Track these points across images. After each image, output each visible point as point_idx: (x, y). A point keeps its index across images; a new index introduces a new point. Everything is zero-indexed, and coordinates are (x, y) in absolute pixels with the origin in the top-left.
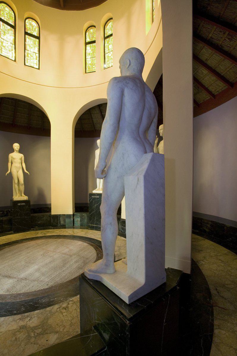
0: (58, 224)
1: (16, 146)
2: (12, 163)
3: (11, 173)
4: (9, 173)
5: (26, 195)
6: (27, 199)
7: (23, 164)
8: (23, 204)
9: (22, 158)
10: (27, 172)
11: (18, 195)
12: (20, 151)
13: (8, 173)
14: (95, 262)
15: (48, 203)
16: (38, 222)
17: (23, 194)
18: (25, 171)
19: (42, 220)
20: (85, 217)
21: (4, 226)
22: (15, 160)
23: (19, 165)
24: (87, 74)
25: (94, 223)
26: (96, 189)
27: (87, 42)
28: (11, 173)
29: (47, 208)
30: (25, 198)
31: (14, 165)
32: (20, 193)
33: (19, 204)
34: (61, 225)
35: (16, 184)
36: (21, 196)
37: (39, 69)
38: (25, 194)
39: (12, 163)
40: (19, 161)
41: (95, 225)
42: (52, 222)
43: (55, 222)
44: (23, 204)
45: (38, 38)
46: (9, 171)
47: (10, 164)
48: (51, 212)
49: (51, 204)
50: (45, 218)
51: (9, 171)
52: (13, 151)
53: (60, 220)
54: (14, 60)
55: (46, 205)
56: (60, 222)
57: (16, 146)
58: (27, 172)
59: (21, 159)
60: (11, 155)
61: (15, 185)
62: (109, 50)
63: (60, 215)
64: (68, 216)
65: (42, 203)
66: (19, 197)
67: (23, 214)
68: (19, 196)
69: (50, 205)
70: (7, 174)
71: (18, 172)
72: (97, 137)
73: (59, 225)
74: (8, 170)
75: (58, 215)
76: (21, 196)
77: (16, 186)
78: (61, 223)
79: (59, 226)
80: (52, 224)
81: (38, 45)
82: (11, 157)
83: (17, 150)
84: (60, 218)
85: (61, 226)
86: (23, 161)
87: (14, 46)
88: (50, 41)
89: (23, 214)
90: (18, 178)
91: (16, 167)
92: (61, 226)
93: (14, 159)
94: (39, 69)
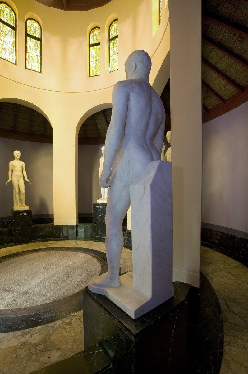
0: (61, 235)
1: (17, 153)
2: (12, 172)
3: (11, 182)
4: (10, 182)
5: (27, 205)
6: (29, 209)
7: (24, 172)
8: (24, 214)
9: (23, 166)
10: (28, 181)
11: (19, 204)
12: (21, 159)
13: (8, 181)
14: (99, 275)
15: (50, 213)
16: (40, 233)
17: (24, 204)
18: (27, 179)
19: (44, 232)
20: (89, 228)
21: (4, 237)
22: (16, 168)
23: (20, 173)
24: (91, 77)
25: (99, 234)
26: (101, 199)
27: (91, 44)
28: (11, 182)
29: (49, 219)
30: (26, 208)
31: (14, 173)
32: (21, 203)
33: (20, 215)
34: (64, 236)
35: (17, 193)
36: (22, 206)
37: (41, 72)
38: (26, 204)
39: (12, 172)
40: (20, 169)
41: (99, 237)
42: (54, 233)
43: (58, 233)
44: (24, 214)
45: (40, 40)
46: (9, 180)
47: (10, 172)
48: (53, 223)
49: (53, 214)
50: (47, 229)
51: (9, 180)
52: (13, 158)
53: (63, 231)
54: (14, 63)
55: (48, 215)
56: (63, 233)
57: (17, 153)
58: (28, 181)
59: (22, 167)
60: (12, 163)
61: (15, 194)
62: (114, 52)
63: (63, 226)
64: (72, 227)
65: (44, 213)
66: (20, 207)
67: (24, 225)
68: (20, 206)
69: (53, 215)
70: (8, 183)
71: (18, 181)
72: (102, 144)
73: (62, 236)
74: (8, 179)
75: (60, 226)
76: (22, 206)
77: (17, 195)
78: (64, 234)
79: (62, 238)
80: (54, 235)
81: (40, 47)
82: (11, 165)
83: (18, 157)
84: (63, 229)
85: (64, 237)
86: (24, 170)
87: (14, 48)
88: (53, 43)
89: (24, 225)
90: (19, 187)
91: (17, 175)
92: (64, 237)
93: (15, 167)
94: (41, 72)
